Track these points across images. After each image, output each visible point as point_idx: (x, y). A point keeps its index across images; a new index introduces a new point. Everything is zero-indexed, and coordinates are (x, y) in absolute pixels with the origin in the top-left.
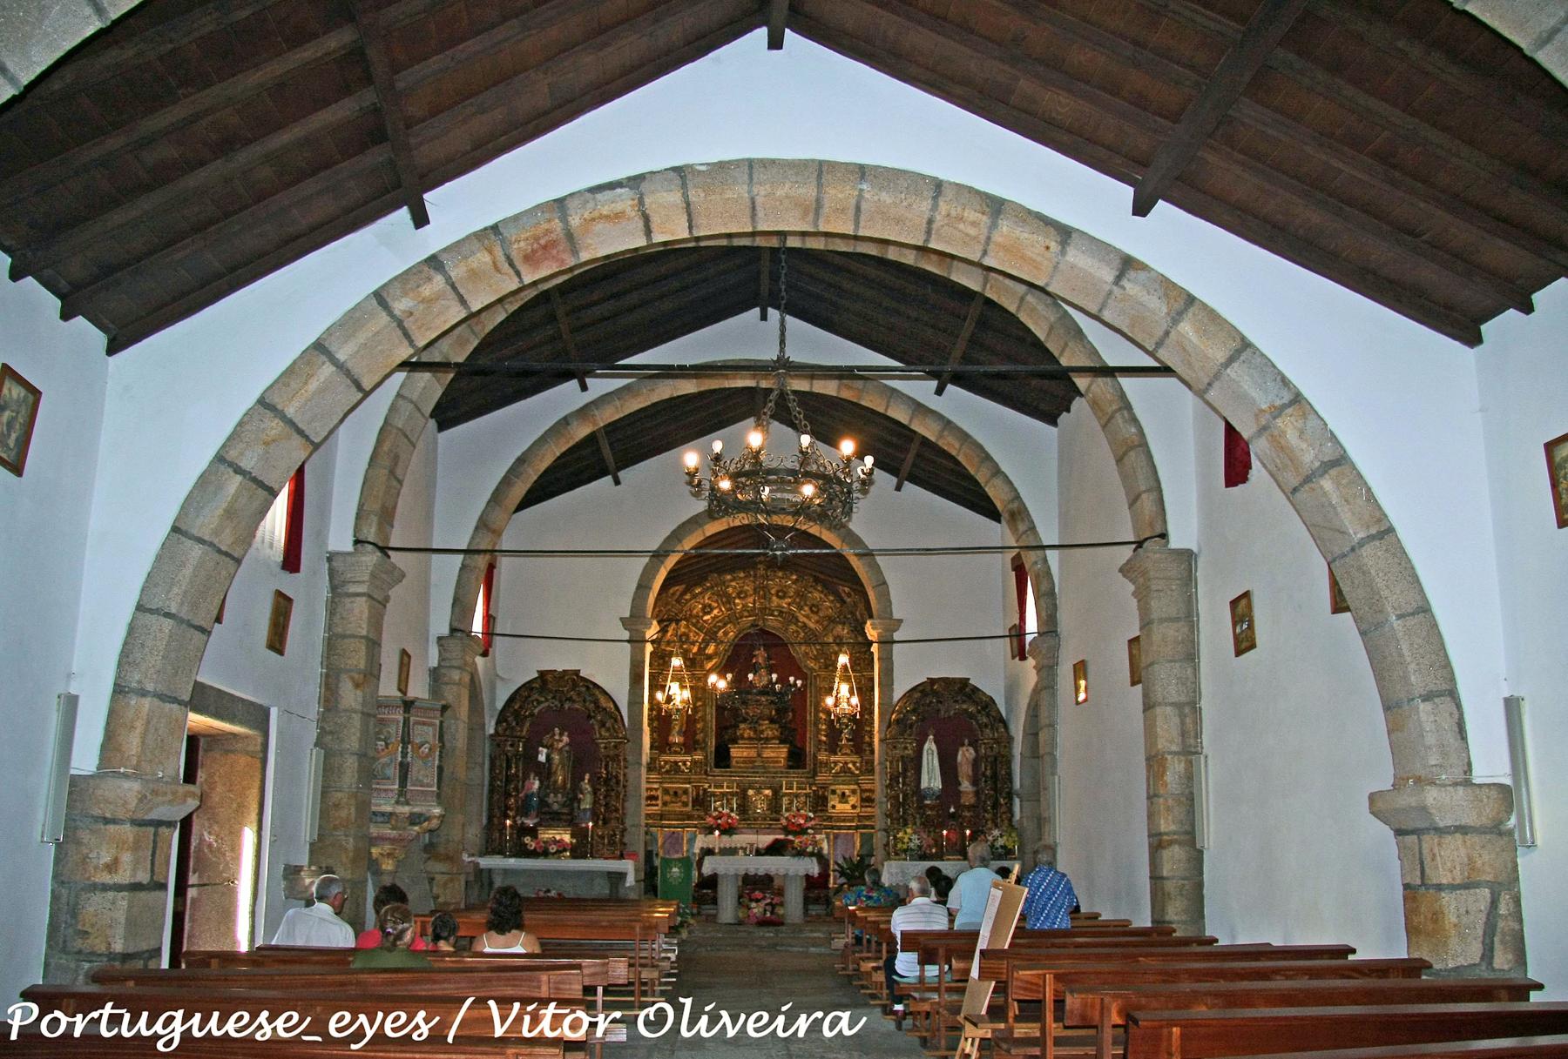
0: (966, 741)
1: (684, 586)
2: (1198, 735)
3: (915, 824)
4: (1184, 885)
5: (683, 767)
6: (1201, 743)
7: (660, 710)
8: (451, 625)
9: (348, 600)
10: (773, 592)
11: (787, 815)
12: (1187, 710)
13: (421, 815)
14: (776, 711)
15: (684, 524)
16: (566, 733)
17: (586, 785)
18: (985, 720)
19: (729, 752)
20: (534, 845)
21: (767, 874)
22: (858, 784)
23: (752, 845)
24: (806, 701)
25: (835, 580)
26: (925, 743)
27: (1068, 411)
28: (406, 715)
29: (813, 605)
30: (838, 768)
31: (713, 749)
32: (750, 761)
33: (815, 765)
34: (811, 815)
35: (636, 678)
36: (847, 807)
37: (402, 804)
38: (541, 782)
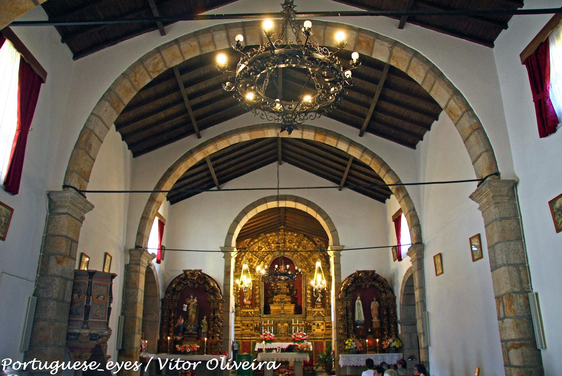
0: (375, 299)
1: (250, 239)
2: (529, 281)
3: (353, 337)
4: (531, 371)
5: (250, 314)
6: (531, 286)
7: (237, 288)
8: (136, 244)
9: (58, 217)
10: (287, 241)
11: (295, 334)
12: (521, 268)
13: (96, 335)
14: (289, 290)
15: (248, 206)
16: (196, 298)
17: (204, 321)
18: (383, 289)
19: (270, 308)
20: (180, 349)
21: (286, 361)
22: (324, 320)
23: (279, 347)
24: (301, 286)
25: (313, 236)
26: (356, 300)
27: (437, 120)
28: (90, 280)
29: (304, 246)
30: (315, 314)
31: (263, 306)
32: (278, 311)
33: (306, 312)
34: (305, 334)
35: (227, 273)
36: (320, 330)
37: (85, 329)
38: (185, 320)
